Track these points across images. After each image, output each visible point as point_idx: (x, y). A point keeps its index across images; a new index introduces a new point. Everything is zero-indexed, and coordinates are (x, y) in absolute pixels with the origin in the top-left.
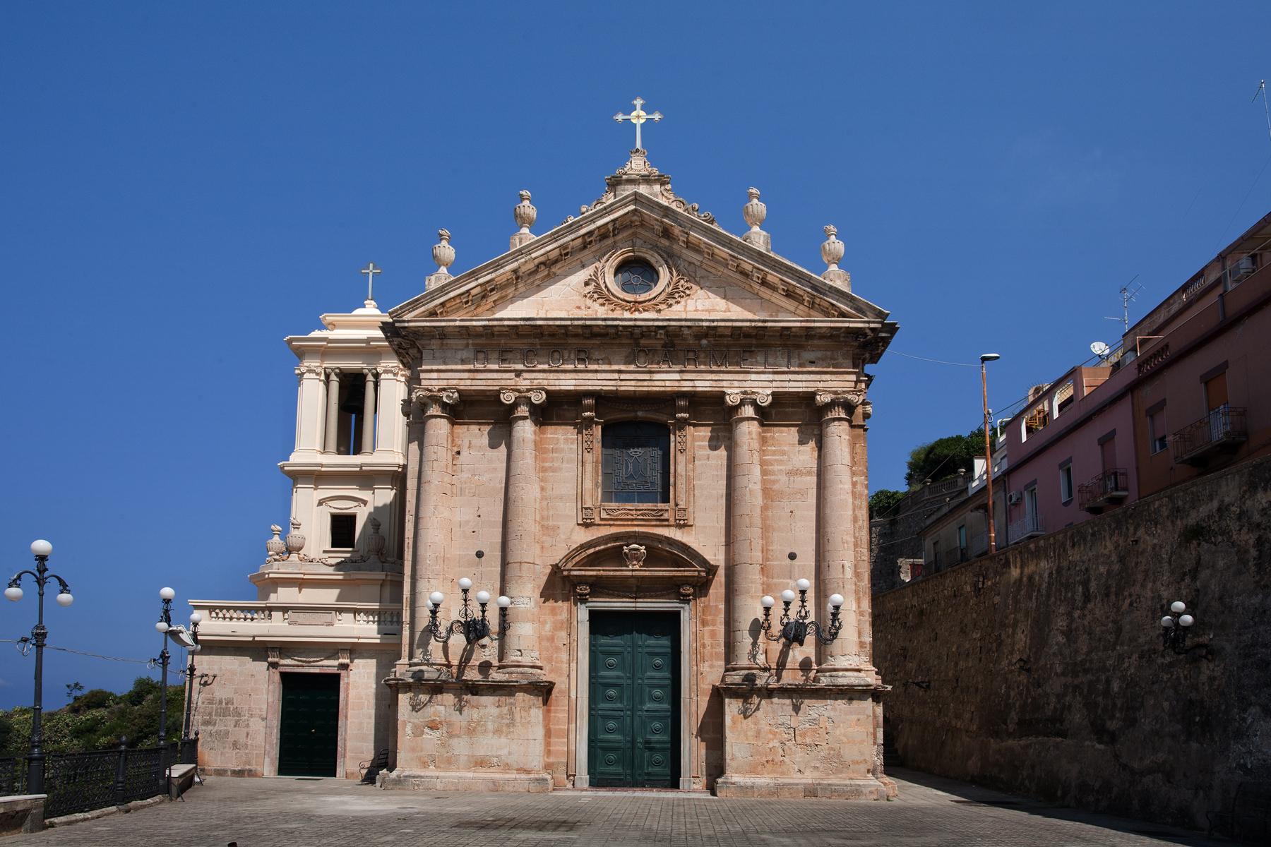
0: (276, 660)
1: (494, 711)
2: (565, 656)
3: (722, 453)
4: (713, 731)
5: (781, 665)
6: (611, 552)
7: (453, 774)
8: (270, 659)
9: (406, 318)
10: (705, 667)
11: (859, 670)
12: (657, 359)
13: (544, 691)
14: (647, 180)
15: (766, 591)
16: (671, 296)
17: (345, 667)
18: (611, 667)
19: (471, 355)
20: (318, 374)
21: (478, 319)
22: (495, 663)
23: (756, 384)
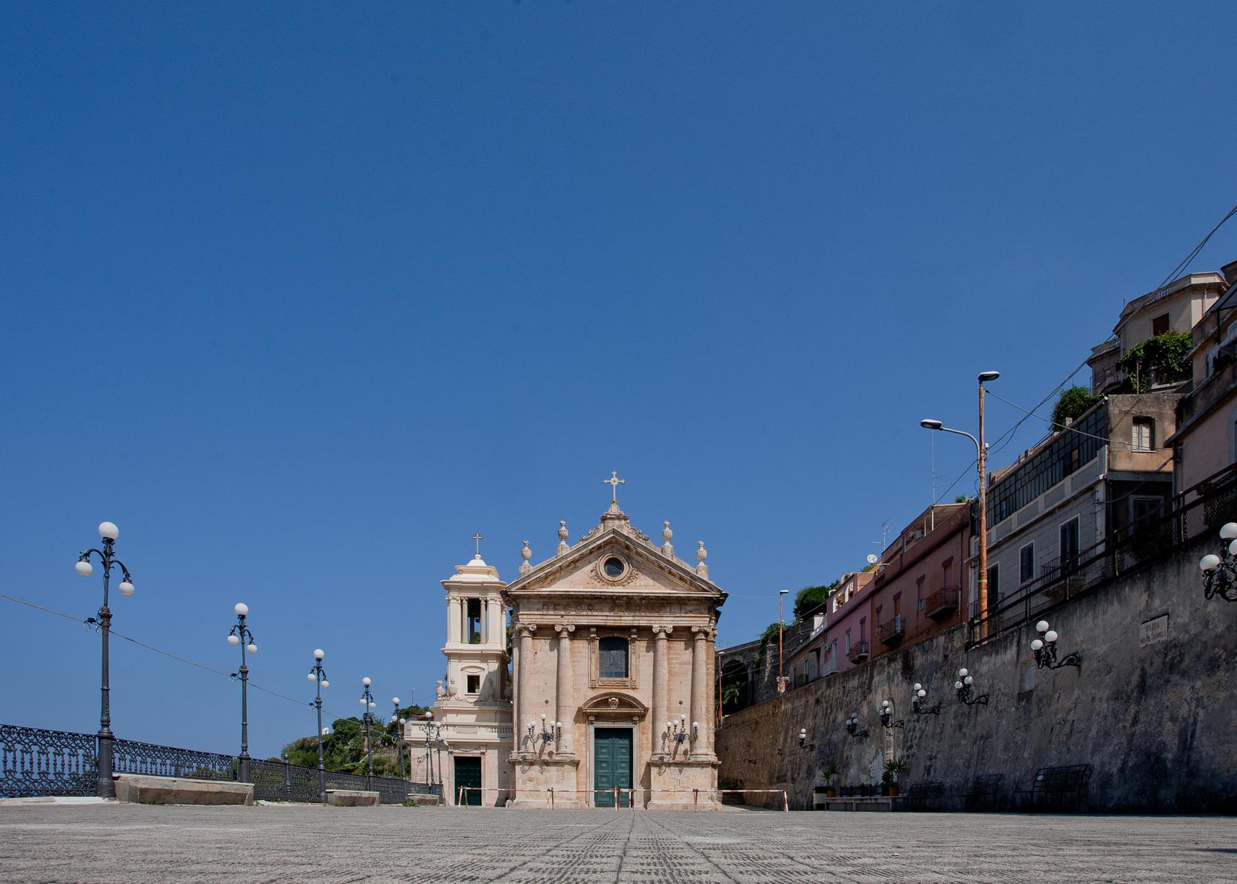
0: (452, 750)
1: (556, 773)
2: (584, 749)
3: (652, 654)
4: (646, 782)
5: (675, 753)
6: (603, 701)
7: (539, 801)
8: (449, 750)
9: (512, 590)
10: (643, 753)
11: (707, 755)
12: (623, 610)
13: (576, 764)
14: (618, 518)
15: (670, 719)
16: (629, 578)
17: (483, 753)
18: (603, 754)
19: (541, 607)
20: (457, 600)
21: (546, 590)
22: (555, 752)
23: (665, 622)
